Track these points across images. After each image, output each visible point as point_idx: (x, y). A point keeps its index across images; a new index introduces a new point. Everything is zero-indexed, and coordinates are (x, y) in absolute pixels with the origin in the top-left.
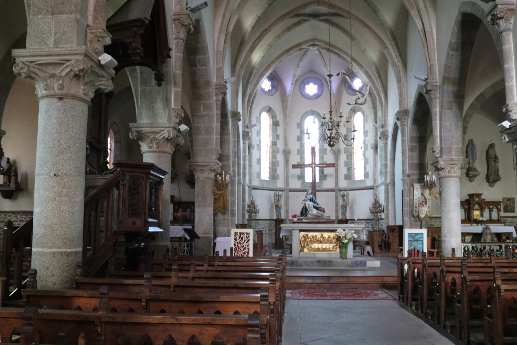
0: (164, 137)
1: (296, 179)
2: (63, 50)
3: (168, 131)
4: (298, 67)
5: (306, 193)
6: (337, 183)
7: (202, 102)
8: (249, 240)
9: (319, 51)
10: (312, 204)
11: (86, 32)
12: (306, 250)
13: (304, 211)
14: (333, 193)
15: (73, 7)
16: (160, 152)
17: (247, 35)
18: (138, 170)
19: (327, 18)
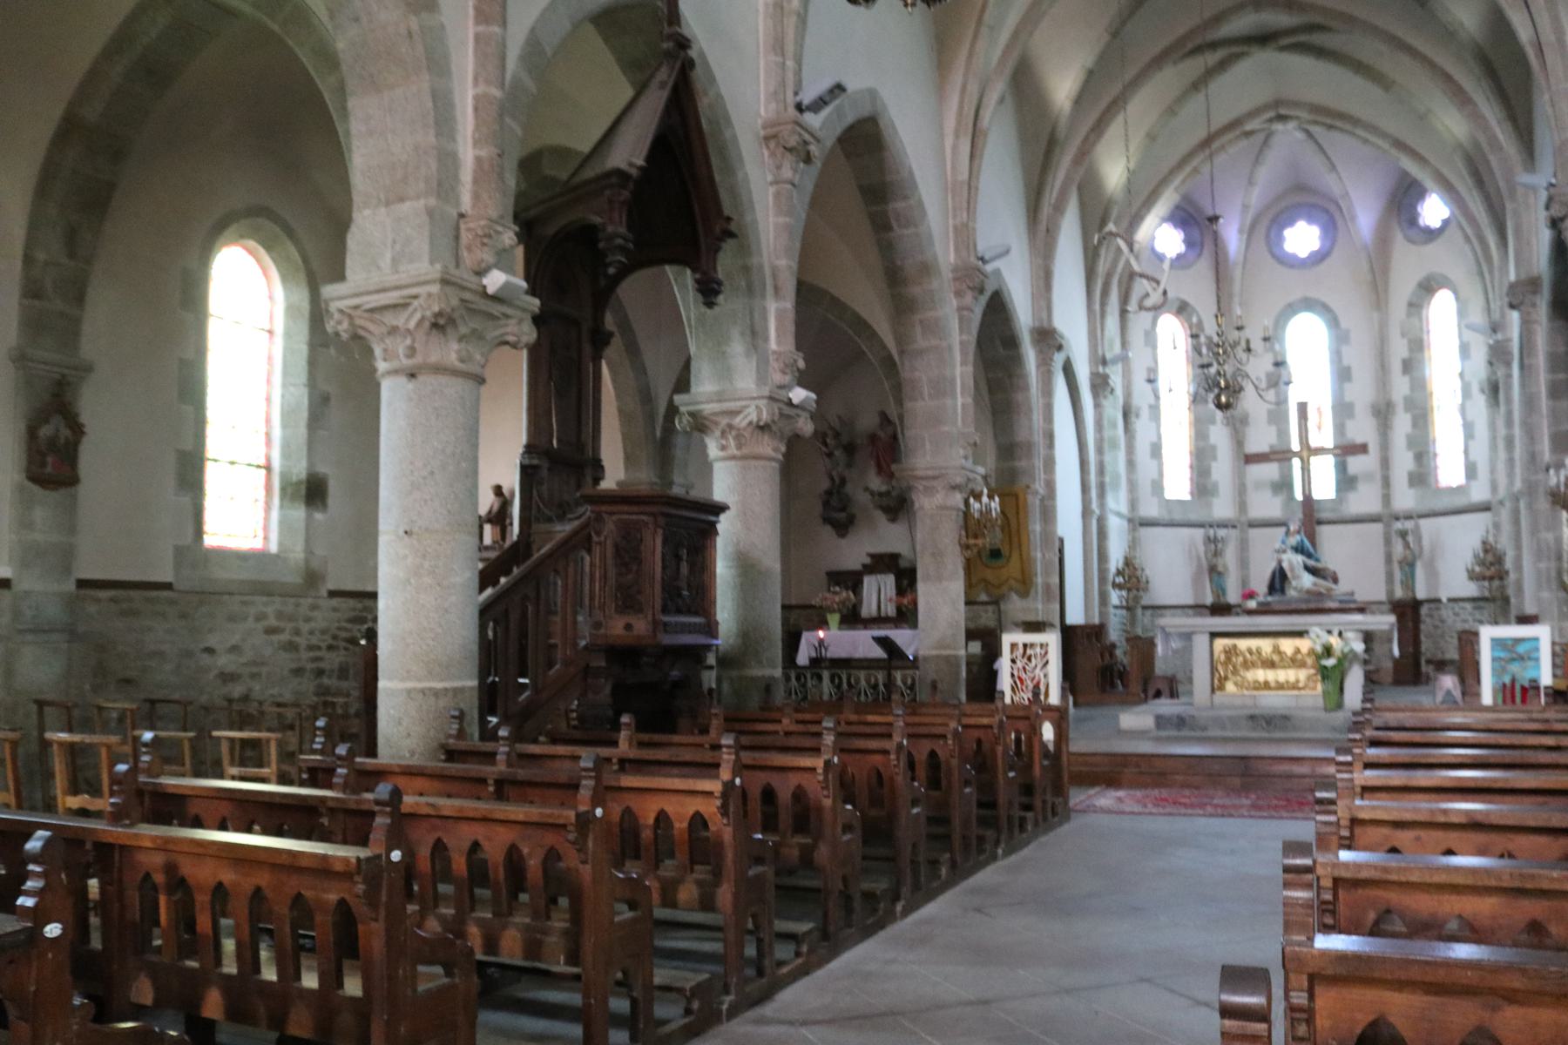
0: (750, 423)
1: (1268, 494)
2: (403, 278)
3: (757, 407)
4: (1251, 182)
5: (1282, 530)
6: (1386, 499)
7: (917, 317)
8: (1047, 662)
9: (1307, 132)
10: (1299, 559)
11: (457, 229)
12: (1230, 687)
13: (1277, 580)
14: (1378, 528)
15: (422, 185)
16: (744, 458)
17: (1063, 122)
18: (635, 509)
19: (1303, 38)
